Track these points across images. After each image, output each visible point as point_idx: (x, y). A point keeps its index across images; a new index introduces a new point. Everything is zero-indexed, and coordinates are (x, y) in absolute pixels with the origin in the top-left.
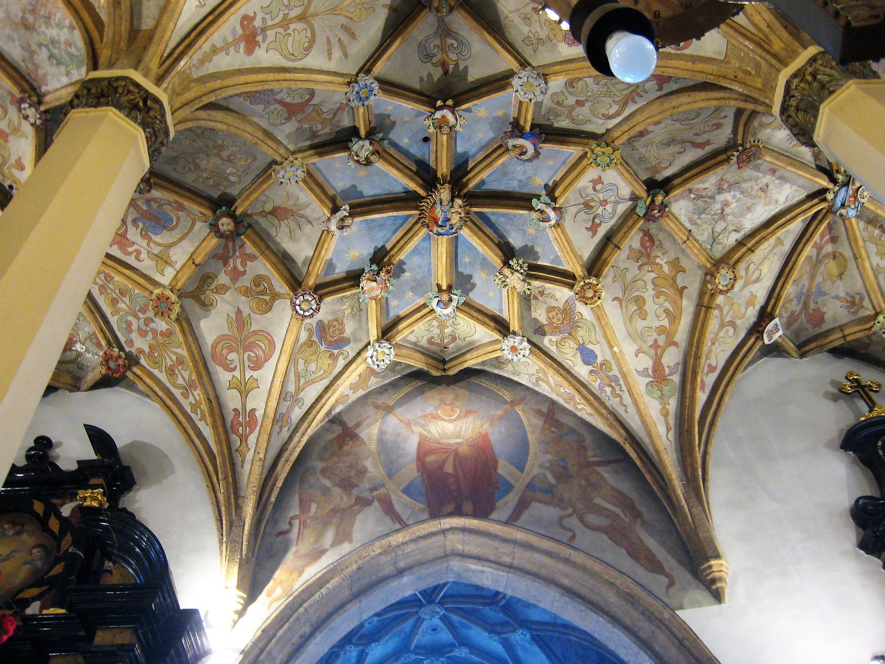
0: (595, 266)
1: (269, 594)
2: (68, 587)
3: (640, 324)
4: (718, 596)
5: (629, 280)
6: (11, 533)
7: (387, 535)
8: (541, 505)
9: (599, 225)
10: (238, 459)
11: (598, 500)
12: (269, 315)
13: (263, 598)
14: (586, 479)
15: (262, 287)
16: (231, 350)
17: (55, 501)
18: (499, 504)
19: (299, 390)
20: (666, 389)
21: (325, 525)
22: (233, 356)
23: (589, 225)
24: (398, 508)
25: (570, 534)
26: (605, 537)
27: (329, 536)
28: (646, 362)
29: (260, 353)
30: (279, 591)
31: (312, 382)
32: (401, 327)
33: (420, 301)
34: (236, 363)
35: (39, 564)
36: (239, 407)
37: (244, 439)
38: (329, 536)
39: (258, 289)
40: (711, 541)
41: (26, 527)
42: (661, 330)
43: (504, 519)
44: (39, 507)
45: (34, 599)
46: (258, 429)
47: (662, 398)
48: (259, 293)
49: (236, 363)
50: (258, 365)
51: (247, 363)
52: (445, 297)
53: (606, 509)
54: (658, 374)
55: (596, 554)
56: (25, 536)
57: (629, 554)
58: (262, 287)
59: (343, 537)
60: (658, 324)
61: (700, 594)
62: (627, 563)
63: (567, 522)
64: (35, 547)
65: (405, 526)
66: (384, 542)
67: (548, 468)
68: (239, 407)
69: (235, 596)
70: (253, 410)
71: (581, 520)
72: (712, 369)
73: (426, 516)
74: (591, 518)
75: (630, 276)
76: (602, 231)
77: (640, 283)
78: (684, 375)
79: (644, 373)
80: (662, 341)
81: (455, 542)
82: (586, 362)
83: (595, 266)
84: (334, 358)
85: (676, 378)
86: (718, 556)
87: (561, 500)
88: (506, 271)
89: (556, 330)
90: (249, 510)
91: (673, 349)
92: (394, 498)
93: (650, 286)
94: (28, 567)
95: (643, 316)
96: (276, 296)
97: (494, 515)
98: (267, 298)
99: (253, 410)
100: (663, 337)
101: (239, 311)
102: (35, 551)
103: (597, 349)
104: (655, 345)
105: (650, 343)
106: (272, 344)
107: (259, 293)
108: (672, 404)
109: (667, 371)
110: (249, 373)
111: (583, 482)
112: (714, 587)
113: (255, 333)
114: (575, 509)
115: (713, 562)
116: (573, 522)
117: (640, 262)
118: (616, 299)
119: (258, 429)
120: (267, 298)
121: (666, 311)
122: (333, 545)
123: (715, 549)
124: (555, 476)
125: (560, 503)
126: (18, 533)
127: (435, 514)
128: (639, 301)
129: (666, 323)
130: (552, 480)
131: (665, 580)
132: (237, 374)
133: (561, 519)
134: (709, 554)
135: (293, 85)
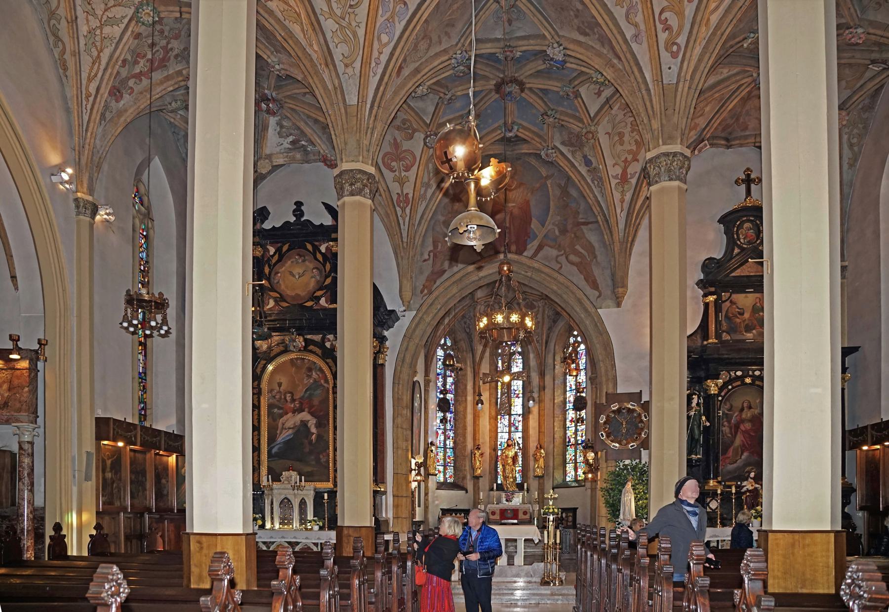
3: (619, 148)
5: (617, 122)
6: (300, 261)
8: (549, 249)
9: (603, 91)
11: (578, 247)
14: (575, 234)
15: (406, 126)
16: (393, 160)
17: (317, 243)
18: (529, 247)
22: (394, 164)
23: (596, 91)
25: (560, 266)
26: (575, 268)
28: (618, 171)
29: (408, 162)
34: (396, 168)
35: (318, 278)
36: (400, 192)
39: (405, 126)
41: (306, 258)
42: (630, 152)
43: (530, 256)
44: (309, 247)
45: (322, 296)
46: (410, 205)
47: (623, 193)
48: (405, 129)
49: (396, 168)
50: (407, 169)
51: (402, 168)
53: (581, 253)
55: (569, 278)
56: (307, 263)
57: (585, 278)
58: (406, 126)
60: (629, 148)
62: (583, 283)
63: (559, 259)
64: (314, 269)
67: (557, 225)
68: (400, 192)
70: (407, 194)
71: (567, 258)
74: (573, 258)
75: (618, 119)
77: (623, 124)
80: (630, 157)
82: (587, 165)
87: (559, 246)
93: (629, 125)
94: (313, 279)
97: (525, 254)
98: (410, 131)
99: (407, 194)
100: (631, 156)
101: (395, 139)
102: (314, 271)
103: (593, 160)
104: (626, 161)
105: (623, 159)
106: (415, 158)
107: (405, 129)
109: (629, 176)
110: (403, 174)
111: (573, 235)
113: (405, 151)
114: (565, 253)
116: (563, 259)
117: (626, 111)
118: (606, 133)
119: (410, 205)
120: (410, 131)
121: (636, 141)
122: (449, 268)
124: (559, 232)
125: (559, 247)
126: (304, 261)
128: (621, 135)
129: (634, 148)
130: (557, 233)
131: (597, 293)
132: (397, 173)
133: (557, 256)
135: (424, 18)
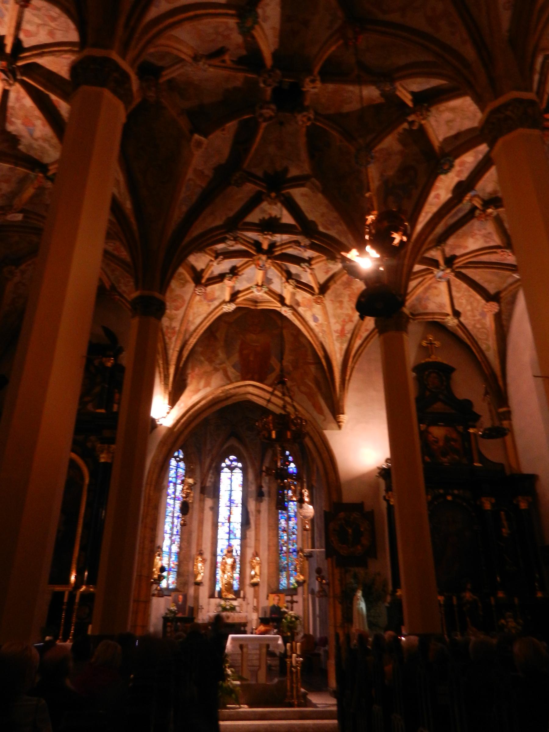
0: (324, 288)
1: (179, 405)
2: (297, 563)
3: (339, 311)
4: (340, 427)
7: (224, 386)
10: (168, 346)
12: (184, 289)
13: (176, 407)
19: (194, 319)
20: (344, 339)
21: (201, 378)
23: (325, 271)
24: (230, 374)
27: (202, 383)
28: (338, 327)
30: (182, 405)
31: (199, 315)
32: (240, 295)
33: (248, 285)
37: (170, 338)
38: (202, 383)
40: (343, 407)
42: (348, 315)
52: (259, 288)
54: (342, 333)
59: (207, 384)
61: (335, 425)
65: (231, 382)
66: (223, 388)
69: (167, 407)
72: (367, 330)
73: (239, 379)
74: (303, 388)
76: (331, 273)
78: (353, 334)
79: (336, 332)
81: (251, 390)
83: (324, 288)
84: (209, 305)
85: (349, 336)
86: (343, 414)
88: (287, 284)
89: (305, 306)
90: (172, 371)
91: (350, 323)
92: (228, 369)
95: (341, 307)
96: (187, 281)
105: (342, 319)
108: (345, 346)
112: (339, 424)
113: (177, 295)
115: (341, 416)
123: (343, 410)
127: (244, 379)
128: (341, 302)
134: (341, 412)
